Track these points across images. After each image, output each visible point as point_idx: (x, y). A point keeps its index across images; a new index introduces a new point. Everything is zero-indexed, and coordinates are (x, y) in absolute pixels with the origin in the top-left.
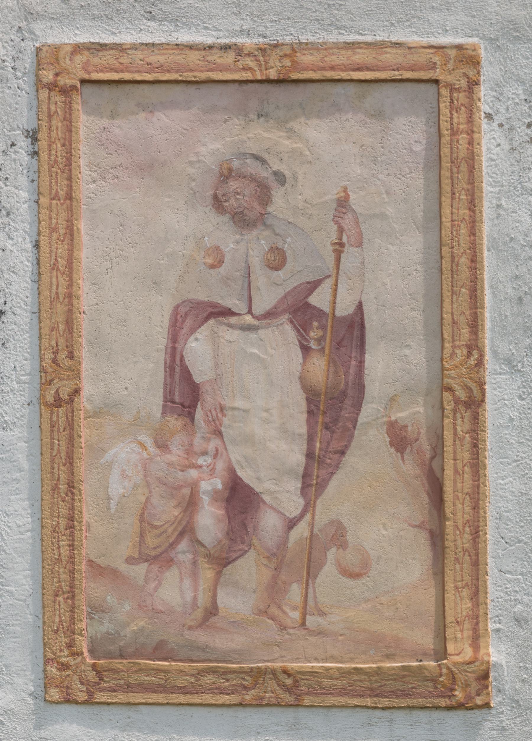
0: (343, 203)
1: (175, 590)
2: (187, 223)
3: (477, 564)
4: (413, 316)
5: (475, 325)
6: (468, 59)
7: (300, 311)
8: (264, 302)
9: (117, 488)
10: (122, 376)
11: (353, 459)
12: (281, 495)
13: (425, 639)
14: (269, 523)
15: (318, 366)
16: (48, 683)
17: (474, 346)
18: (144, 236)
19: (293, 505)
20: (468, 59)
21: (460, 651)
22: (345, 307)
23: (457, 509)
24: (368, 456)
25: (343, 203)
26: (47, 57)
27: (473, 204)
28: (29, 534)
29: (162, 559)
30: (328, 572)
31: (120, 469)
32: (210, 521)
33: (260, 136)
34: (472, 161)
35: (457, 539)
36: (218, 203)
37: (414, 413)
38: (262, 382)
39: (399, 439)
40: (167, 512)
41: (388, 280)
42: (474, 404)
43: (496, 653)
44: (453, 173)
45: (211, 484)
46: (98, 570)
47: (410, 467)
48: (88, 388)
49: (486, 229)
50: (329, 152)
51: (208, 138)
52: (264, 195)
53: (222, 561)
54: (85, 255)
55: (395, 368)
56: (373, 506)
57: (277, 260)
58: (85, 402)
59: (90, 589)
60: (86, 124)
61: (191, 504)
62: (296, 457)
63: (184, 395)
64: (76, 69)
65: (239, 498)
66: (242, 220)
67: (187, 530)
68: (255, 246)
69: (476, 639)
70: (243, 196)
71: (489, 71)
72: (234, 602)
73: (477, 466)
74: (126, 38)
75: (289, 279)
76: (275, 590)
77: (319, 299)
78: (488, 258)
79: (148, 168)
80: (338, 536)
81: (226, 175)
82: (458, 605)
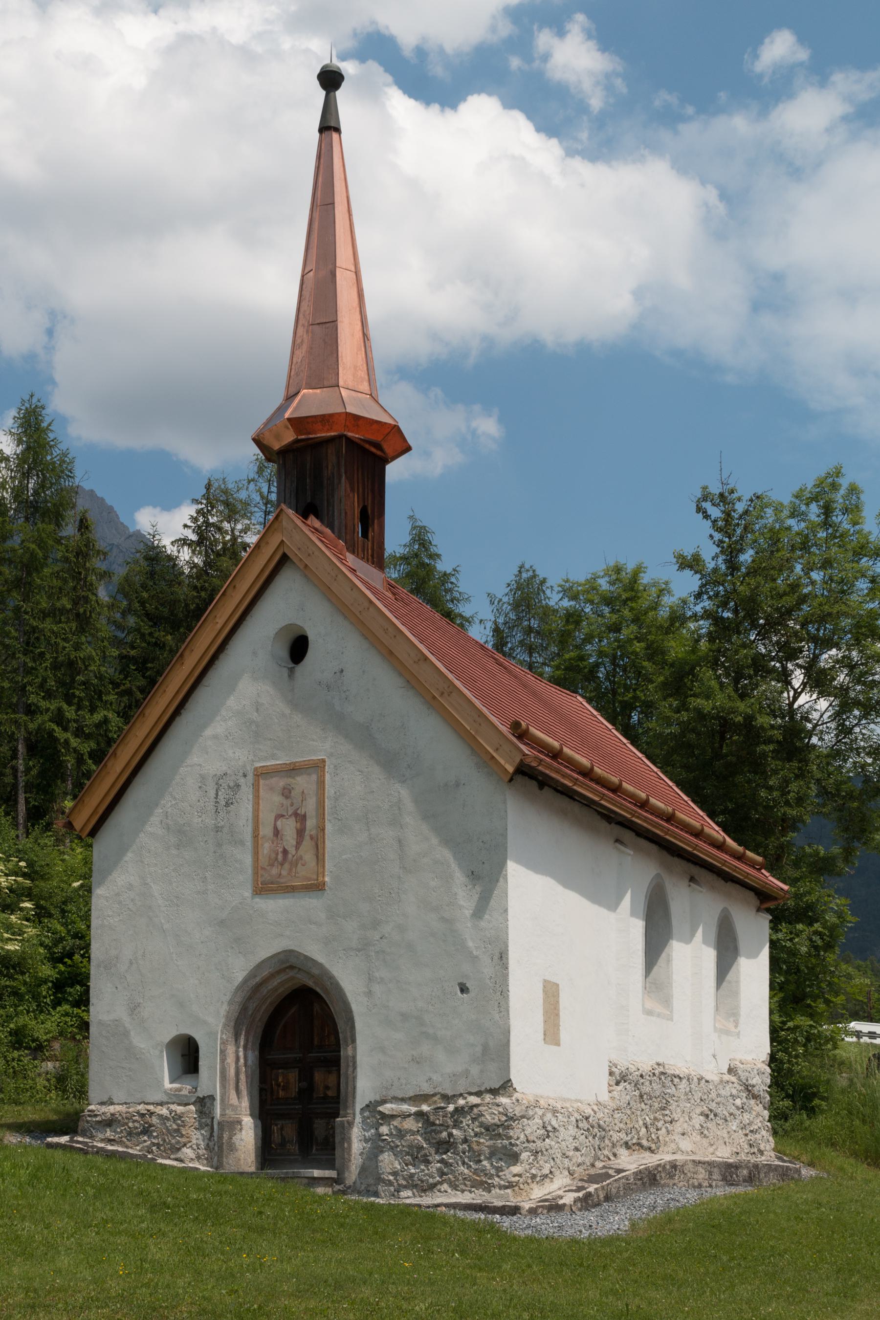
0: (303, 792)
1: (275, 871)
2: (277, 799)
3: (324, 861)
4: (314, 813)
5: (324, 814)
6: (323, 761)
7: (296, 814)
8: (290, 813)
9: (265, 852)
10: (266, 831)
11: (304, 843)
12: (292, 851)
13: (315, 877)
14: (290, 856)
15: (299, 824)
16: (254, 891)
17: (324, 818)
18: (271, 801)
19: (294, 852)
20: (323, 761)
21: (321, 879)
22: (303, 813)
23: (321, 851)
24: (307, 843)
25: (303, 792)
26: (256, 769)
27: (324, 790)
28: (192, 1108)
29: (272, 865)
30: (299, 865)
31: (266, 848)
32: (280, 857)
33: (290, 780)
34: (324, 782)
35: (320, 857)
36: (283, 794)
37: (314, 832)
38: (289, 828)
39: (312, 838)
40: (273, 856)
41: (310, 807)
42: (323, 830)
43: (326, 879)
44: (321, 783)
45: (281, 850)
46: (262, 868)
47: (313, 843)
48: (261, 833)
49: (326, 795)
50: (303, 783)
51: (280, 782)
52: (290, 793)
53: (282, 865)
54: (260, 807)
55: (311, 823)
56: (307, 853)
57: (292, 805)
58: (260, 836)
59: (261, 872)
60: (262, 782)
61: (277, 854)
62: (295, 843)
63: (277, 832)
64: (260, 771)
65: (285, 852)
66: (287, 797)
67: (276, 859)
68: (289, 802)
69: (323, 876)
70: (287, 793)
71: (327, 763)
72: (284, 873)
73: (324, 842)
74: (268, 764)
75: (294, 808)
76: (291, 870)
77: (299, 812)
78: (326, 800)
79: (272, 789)
80: (301, 858)
81: (284, 788)
82: (321, 870)
